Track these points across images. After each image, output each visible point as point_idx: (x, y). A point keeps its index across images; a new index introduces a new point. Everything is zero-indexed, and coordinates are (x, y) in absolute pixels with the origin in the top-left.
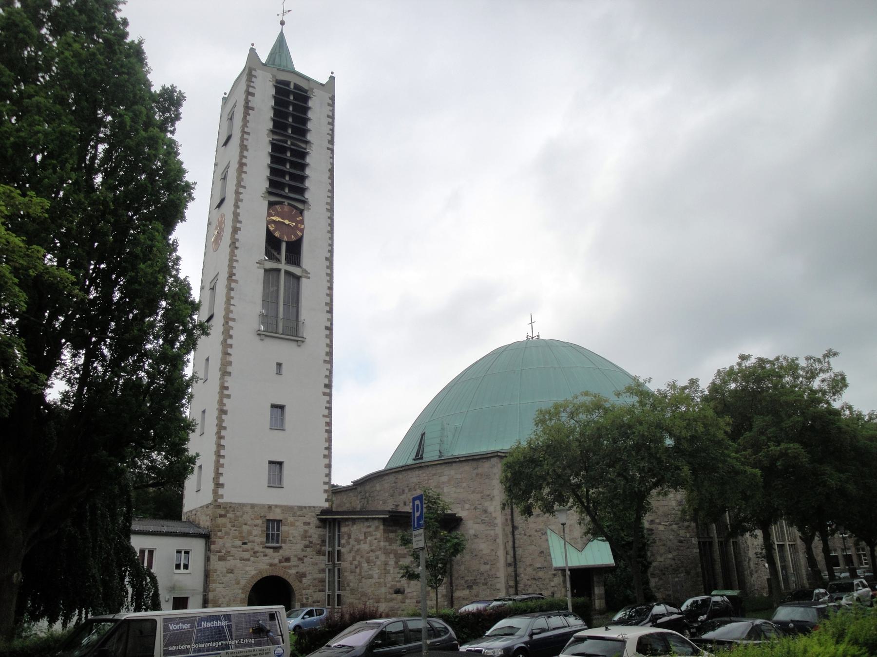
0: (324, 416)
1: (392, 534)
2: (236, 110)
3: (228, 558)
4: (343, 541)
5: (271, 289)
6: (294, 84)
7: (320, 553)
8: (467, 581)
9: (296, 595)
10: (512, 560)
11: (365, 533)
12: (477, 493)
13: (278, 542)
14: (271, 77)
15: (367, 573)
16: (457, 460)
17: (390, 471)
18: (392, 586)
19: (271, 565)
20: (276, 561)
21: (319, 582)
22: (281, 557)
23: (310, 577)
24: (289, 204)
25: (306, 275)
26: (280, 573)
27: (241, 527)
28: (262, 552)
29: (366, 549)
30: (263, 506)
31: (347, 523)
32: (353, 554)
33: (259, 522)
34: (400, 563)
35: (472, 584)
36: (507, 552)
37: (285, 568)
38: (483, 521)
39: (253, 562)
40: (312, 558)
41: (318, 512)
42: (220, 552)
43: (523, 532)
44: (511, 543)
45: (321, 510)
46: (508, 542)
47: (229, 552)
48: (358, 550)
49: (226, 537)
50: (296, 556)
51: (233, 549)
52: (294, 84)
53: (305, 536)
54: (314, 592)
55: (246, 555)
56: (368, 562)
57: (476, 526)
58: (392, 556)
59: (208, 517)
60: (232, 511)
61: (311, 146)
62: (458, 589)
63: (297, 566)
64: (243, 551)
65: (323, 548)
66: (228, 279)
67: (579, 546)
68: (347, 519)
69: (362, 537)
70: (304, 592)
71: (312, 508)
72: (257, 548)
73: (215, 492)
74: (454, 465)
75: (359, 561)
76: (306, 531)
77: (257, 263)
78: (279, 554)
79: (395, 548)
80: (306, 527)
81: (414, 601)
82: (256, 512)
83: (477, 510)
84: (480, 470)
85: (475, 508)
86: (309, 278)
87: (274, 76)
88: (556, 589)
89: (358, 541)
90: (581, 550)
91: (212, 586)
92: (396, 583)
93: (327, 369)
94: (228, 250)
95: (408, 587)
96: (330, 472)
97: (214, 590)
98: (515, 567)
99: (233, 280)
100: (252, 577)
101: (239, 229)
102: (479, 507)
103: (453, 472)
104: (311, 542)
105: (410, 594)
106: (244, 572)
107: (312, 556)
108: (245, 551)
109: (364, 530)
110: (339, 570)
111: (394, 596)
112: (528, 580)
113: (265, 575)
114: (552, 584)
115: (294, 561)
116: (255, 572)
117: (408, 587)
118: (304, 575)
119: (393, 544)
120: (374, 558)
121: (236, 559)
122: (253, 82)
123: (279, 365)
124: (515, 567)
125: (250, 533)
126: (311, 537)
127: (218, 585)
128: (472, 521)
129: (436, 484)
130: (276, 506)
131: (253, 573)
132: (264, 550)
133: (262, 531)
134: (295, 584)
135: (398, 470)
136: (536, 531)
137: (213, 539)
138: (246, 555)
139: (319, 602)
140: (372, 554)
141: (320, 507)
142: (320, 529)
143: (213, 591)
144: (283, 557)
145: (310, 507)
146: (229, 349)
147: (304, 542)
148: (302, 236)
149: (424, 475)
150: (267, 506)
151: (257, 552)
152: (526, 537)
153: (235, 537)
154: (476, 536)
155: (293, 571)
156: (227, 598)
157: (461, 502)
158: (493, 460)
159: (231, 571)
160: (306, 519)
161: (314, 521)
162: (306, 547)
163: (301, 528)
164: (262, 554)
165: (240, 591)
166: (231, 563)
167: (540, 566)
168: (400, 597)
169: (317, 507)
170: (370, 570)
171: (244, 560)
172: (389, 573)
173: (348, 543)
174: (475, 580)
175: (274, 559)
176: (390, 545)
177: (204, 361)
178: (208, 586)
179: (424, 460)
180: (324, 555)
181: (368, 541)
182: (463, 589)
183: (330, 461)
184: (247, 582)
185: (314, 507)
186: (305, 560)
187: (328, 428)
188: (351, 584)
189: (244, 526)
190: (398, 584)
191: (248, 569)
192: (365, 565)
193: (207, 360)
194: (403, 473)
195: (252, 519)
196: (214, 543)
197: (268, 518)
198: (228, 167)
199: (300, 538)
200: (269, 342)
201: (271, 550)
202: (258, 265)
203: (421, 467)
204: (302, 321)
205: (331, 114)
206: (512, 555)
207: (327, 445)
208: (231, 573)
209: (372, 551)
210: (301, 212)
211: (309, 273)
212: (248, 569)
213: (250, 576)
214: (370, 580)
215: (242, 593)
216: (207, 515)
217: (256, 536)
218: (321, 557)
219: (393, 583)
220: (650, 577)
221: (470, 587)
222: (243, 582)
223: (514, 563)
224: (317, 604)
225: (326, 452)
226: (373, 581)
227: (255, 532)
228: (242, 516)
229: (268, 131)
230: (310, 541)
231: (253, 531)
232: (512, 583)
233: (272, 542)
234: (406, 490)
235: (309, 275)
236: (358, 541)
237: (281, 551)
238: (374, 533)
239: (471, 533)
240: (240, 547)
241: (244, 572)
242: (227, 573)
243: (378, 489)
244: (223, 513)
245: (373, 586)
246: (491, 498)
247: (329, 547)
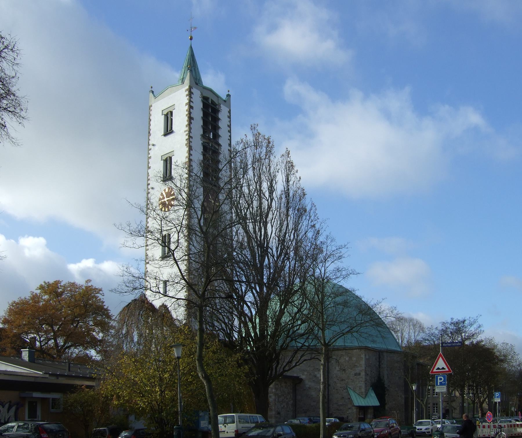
6: (211, 99)
52: (211, 99)
67: (364, 396)
87: (202, 94)
88: (350, 415)
90: (365, 398)
112: (334, 410)
136: (341, 387)
154: (310, 388)
167: (341, 404)
220: (212, 429)
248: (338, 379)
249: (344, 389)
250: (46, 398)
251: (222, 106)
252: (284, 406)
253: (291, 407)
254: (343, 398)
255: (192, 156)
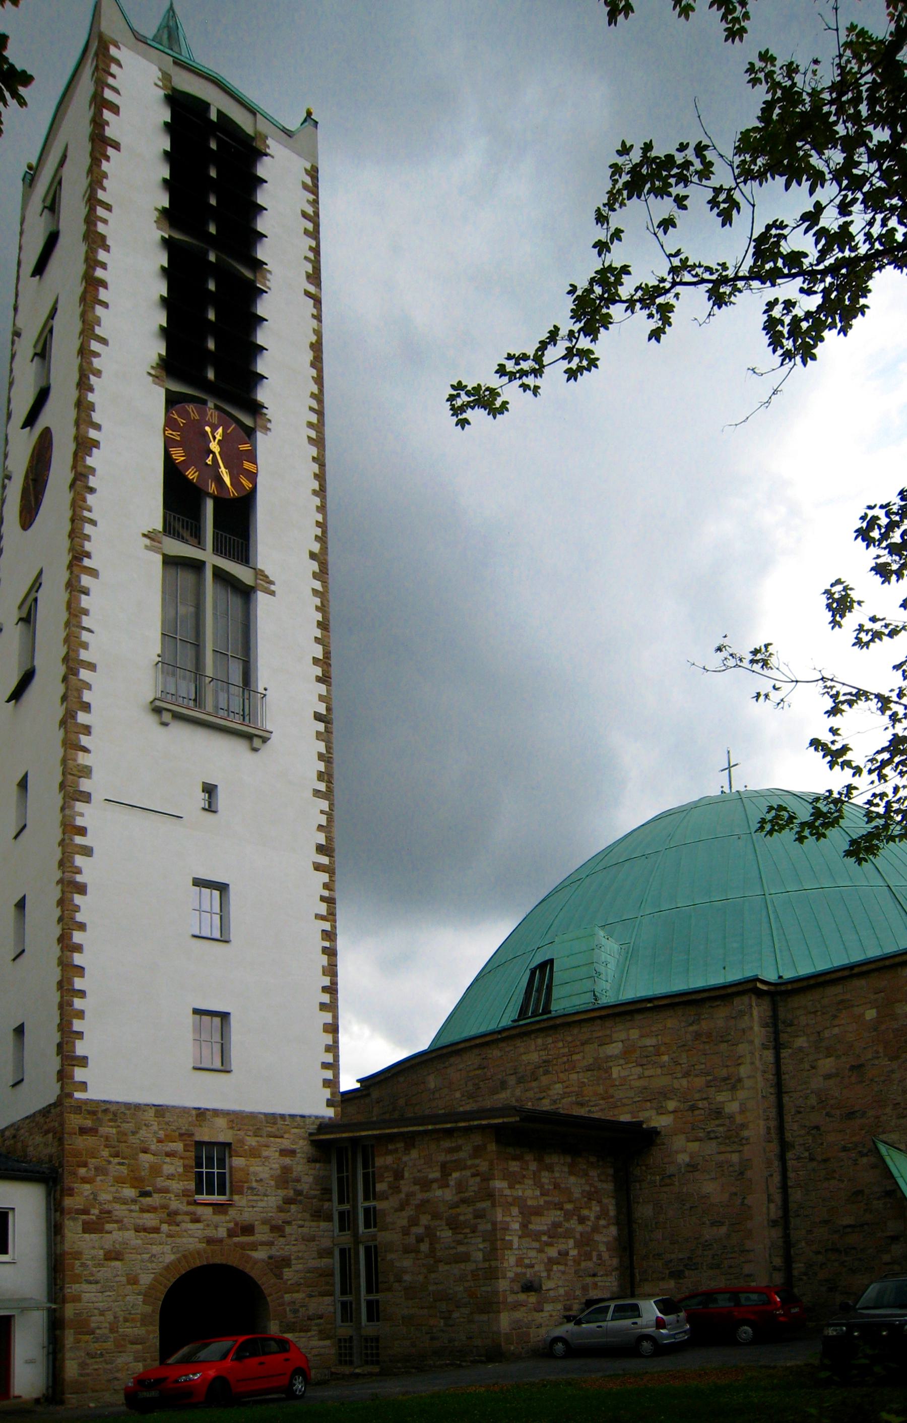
0: (319, 917)
1: (514, 1163)
2: (57, 323)
3: (108, 1227)
4: (380, 1187)
5: (182, 610)
7: (318, 1215)
8: (671, 1261)
9: (270, 1304)
10: (780, 1213)
11: (443, 1166)
12: (697, 1076)
13: (222, 1192)
14: (160, 75)
15: (455, 1251)
16: (649, 1005)
17: (467, 1044)
18: (516, 1274)
19: (210, 1241)
20: (222, 1233)
21: (320, 1275)
22: (231, 1225)
23: (300, 1267)
24: (217, 407)
25: (266, 585)
26: (233, 1261)
27: (135, 1157)
28: (187, 1213)
29: (449, 1198)
30: (185, 1110)
31: (390, 1147)
32: (409, 1212)
33: (179, 1146)
34: (531, 1227)
35: (681, 1268)
36: (769, 1195)
37: (243, 1246)
38: (712, 1135)
39: (169, 1236)
40: (302, 1226)
41: (313, 1128)
42: (86, 1212)
43: (806, 1154)
44: (777, 1179)
45: (318, 1122)
46: (771, 1175)
47: (109, 1212)
48: (425, 1202)
49: (99, 1178)
50: (264, 1222)
51: (117, 1206)
53: (284, 1178)
54: (311, 1296)
55: (150, 1220)
56: (454, 1225)
57: (694, 1146)
58: (515, 1211)
59: (51, 1135)
60: (111, 1120)
61: (265, 278)
62: (647, 1280)
63: (270, 1244)
64: (142, 1210)
65: (326, 1205)
66: (70, 566)
68: (391, 1138)
69: (435, 1174)
70: (287, 1297)
71: (298, 1118)
72: (175, 1205)
73: (63, 1076)
74: (638, 1017)
75: (427, 1228)
76: (286, 1170)
77: (144, 535)
78: (228, 1218)
79: (520, 1193)
80: (287, 1161)
81: (560, 1306)
82: (167, 1123)
83: (697, 1112)
84: (705, 1026)
85: (693, 1108)
86: (273, 593)
87: (166, 77)
89: (426, 1185)
91: (72, 1289)
92: (524, 1270)
93: (322, 812)
94: (68, 496)
95: (549, 1277)
96: (336, 1041)
97: (77, 1299)
98: (786, 1227)
99: (86, 567)
100: (167, 1268)
101: (96, 444)
102: (700, 1104)
103: (634, 1034)
104: (299, 1193)
105: (552, 1293)
106: (146, 1256)
107: (300, 1222)
108: (148, 1211)
109: (442, 1157)
110: (368, 1249)
111: (522, 1297)
113: (198, 1263)
114: (886, 1258)
115: (262, 1234)
116: (173, 1257)
117: (549, 1277)
118: (286, 1262)
119: (517, 1186)
120: (470, 1216)
121: (128, 1230)
122: (114, 76)
123: (210, 790)
124: (786, 1227)
125: (156, 1170)
126: (298, 1180)
127: (85, 1286)
128: (683, 1137)
129: (591, 1061)
130: (216, 1112)
131: (170, 1258)
132: (192, 1208)
133: (185, 1166)
134: (266, 1283)
135: (488, 1039)
136: (845, 1149)
137: (68, 1181)
138: (150, 1220)
139: (321, 1317)
140: (463, 1209)
141: (317, 1117)
142: (318, 1165)
143: (73, 1301)
144: (236, 1224)
145: (292, 1116)
146: (81, 736)
147: (281, 1193)
148: (254, 490)
149: (560, 1044)
150: (194, 1112)
151: (176, 1213)
152: (814, 1164)
153: (120, 1181)
154: (692, 1167)
155: (260, 1254)
156: (110, 1316)
157: (657, 1098)
158: (737, 1001)
159: (113, 1255)
160: (286, 1143)
161: (302, 1146)
162: (288, 1201)
163: (276, 1162)
164: (187, 1218)
165: (140, 1298)
166: (115, 1236)
168: (532, 1298)
169: (310, 1117)
170: (460, 1243)
171: (145, 1230)
172: (511, 1249)
173: (396, 1189)
174: (690, 1258)
175: (216, 1227)
176: (511, 1187)
177: (11, 910)
178: (62, 1288)
179: (553, 1014)
180: (329, 1218)
181: (452, 1183)
182: (663, 1279)
183: (336, 1017)
184: (155, 1279)
185: (303, 1117)
186: (288, 1229)
187: (327, 944)
188: (407, 1278)
189: (142, 1155)
190: (529, 1271)
191: (155, 1249)
192: (446, 1234)
193: (21, 905)
194: (502, 1045)
195: (160, 1141)
196: (71, 1192)
197: (197, 1138)
198: (37, 585)
199: (273, 1183)
200: (181, 733)
201: (210, 1210)
202: (147, 542)
203: (555, 1027)
204: (261, 690)
205: (310, 210)
206: (780, 1203)
207: (326, 981)
208: (117, 1259)
209: (464, 1201)
210: (250, 433)
211: (272, 583)
212: (155, 1249)
213: (161, 1265)
214: (462, 1266)
215: (145, 1302)
216: (47, 1132)
217: (170, 1177)
218: (323, 1225)
219: (519, 1270)
221: (677, 1275)
222: (146, 1279)
223: (784, 1220)
224: (318, 1321)
225: (326, 998)
226: (471, 1266)
227: (168, 1169)
228: (134, 1133)
229: (156, 214)
230: (295, 1190)
231: (165, 1167)
232: (778, 1261)
233: (210, 1192)
234: (512, 1081)
235: (273, 588)
236: (426, 1185)
237: (232, 1212)
238: (469, 1163)
239: (679, 1160)
240: (134, 1201)
241: (146, 1256)
242: (106, 1260)
243: (432, 1085)
244: (89, 1123)
245: (469, 1277)
246: (733, 1084)
247: (341, 1201)
248: (828, 1114)
249: (862, 1154)
250: (324, 1340)
251: (269, 142)
252: (564, 1254)
253: (606, 1256)
254: (860, 1192)
255: (316, 536)
